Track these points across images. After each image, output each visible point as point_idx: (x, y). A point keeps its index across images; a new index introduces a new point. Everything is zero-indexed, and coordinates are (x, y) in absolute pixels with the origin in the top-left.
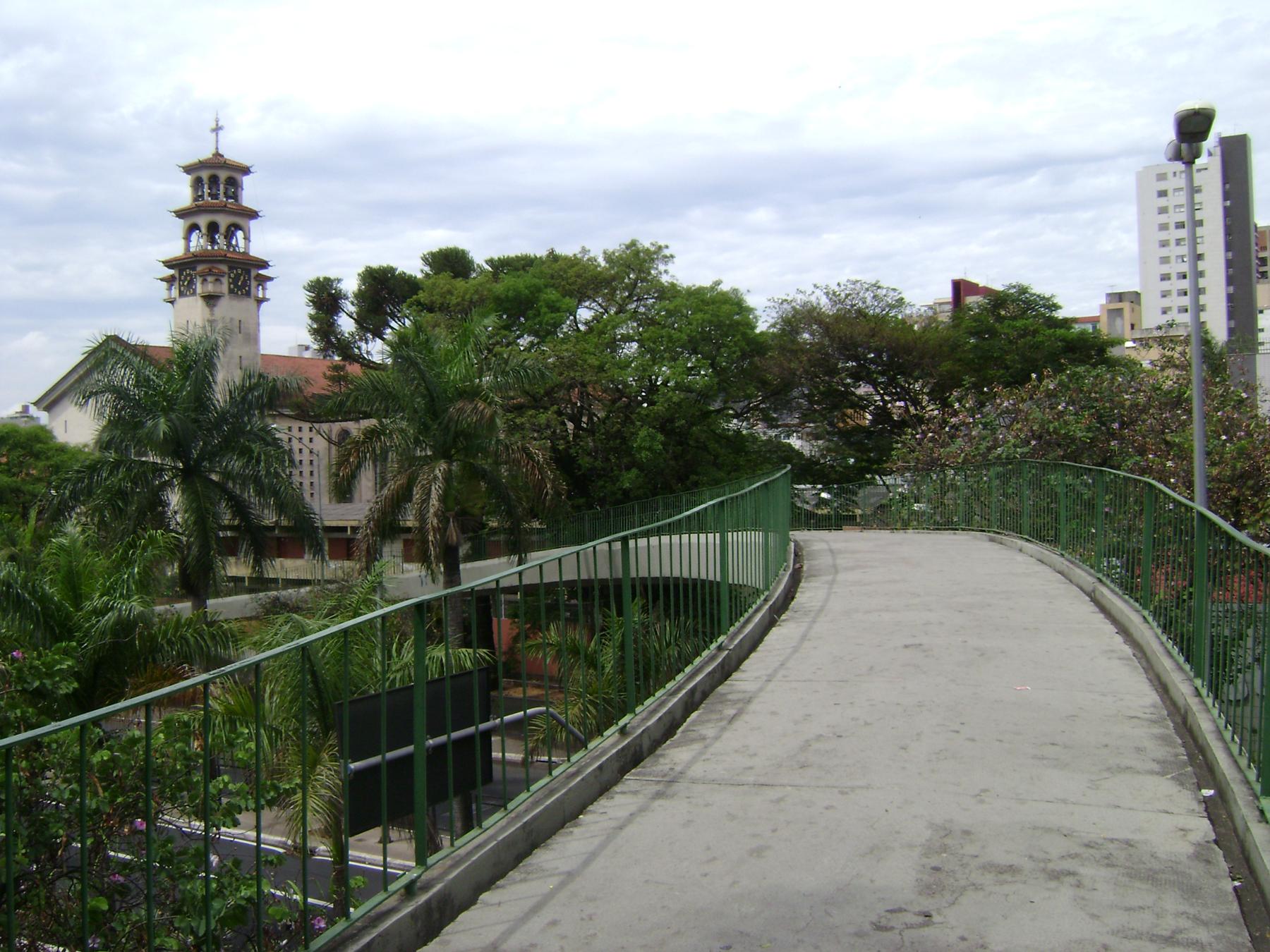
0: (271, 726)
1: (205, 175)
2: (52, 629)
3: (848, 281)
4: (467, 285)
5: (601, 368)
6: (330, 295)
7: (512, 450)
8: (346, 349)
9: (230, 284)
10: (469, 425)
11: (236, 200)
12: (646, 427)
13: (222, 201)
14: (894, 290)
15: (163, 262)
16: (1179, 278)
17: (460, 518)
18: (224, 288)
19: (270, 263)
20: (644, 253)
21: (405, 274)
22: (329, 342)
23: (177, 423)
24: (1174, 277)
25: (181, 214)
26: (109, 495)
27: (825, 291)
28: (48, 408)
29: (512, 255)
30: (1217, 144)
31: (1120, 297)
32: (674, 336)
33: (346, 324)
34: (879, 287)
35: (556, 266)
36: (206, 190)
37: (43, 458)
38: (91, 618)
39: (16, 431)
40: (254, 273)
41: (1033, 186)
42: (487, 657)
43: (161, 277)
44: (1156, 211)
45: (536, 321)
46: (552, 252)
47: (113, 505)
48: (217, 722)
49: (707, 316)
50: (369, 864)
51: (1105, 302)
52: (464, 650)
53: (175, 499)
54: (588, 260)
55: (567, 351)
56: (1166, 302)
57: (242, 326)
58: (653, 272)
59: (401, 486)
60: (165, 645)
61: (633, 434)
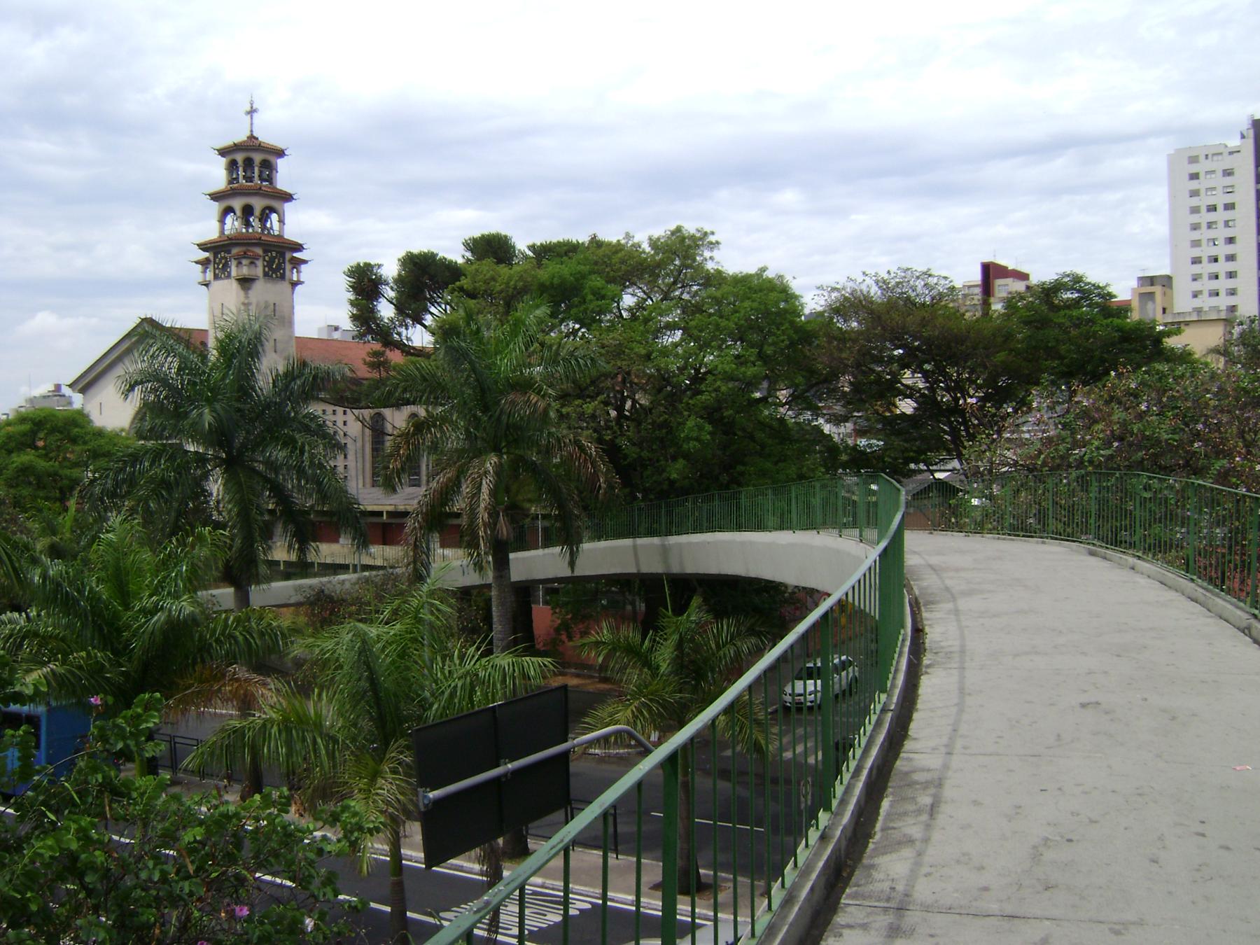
0: (328, 735)
1: (240, 157)
2: (101, 629)
3: (899, 269)
4: (512, 272)
5: (648, 357)
6: (371, 280)
7: (564, 443)
8: (384, 335)
9: (264, 266)
10: (522, 418)
11: (271, 183)
12: (693, 417)
13: (257, 184)
14: (945, 278)
15: (198, 245)
16: (1210, 261)
17: (510, 512)
18: (259, 271)
19: (304, 246)
20: (689, 239)
21: (446, 259)
22: (369, 327)
23: (222, 413)
24: (1205, 260)
25: (216, 197)
26: (153, 486)
27: (874, 278)
28: (83, 391)
29: (555, 240)
30: (1250, 126)
31: (1152, 280)
32: (722, 324)
33: (386, 310)
34: (930, 275)
35: (601, 252)
36: (241, 173)
37: (80, 442)
38: (138, 617)
39: (54, 416)
40: (288, 256)
41: (1060, 167)
42: (551, 666)
43: (196, 260)
44: (1187, 195)
45: (582, 309)
46: (594, 238)
47: (157, 495)
48: (273, 731)
49: (755, 305)
50: (415, 862)
51: (1136, 286)
52: (528, 658)
53: (216, 486)
54: (633, 245)
55: (611, 339)
56: (1197, 286)
57: (277, 308)
58: (698, 258)
59: (450, 480)
60: (214, 644)
61: (679, 424)
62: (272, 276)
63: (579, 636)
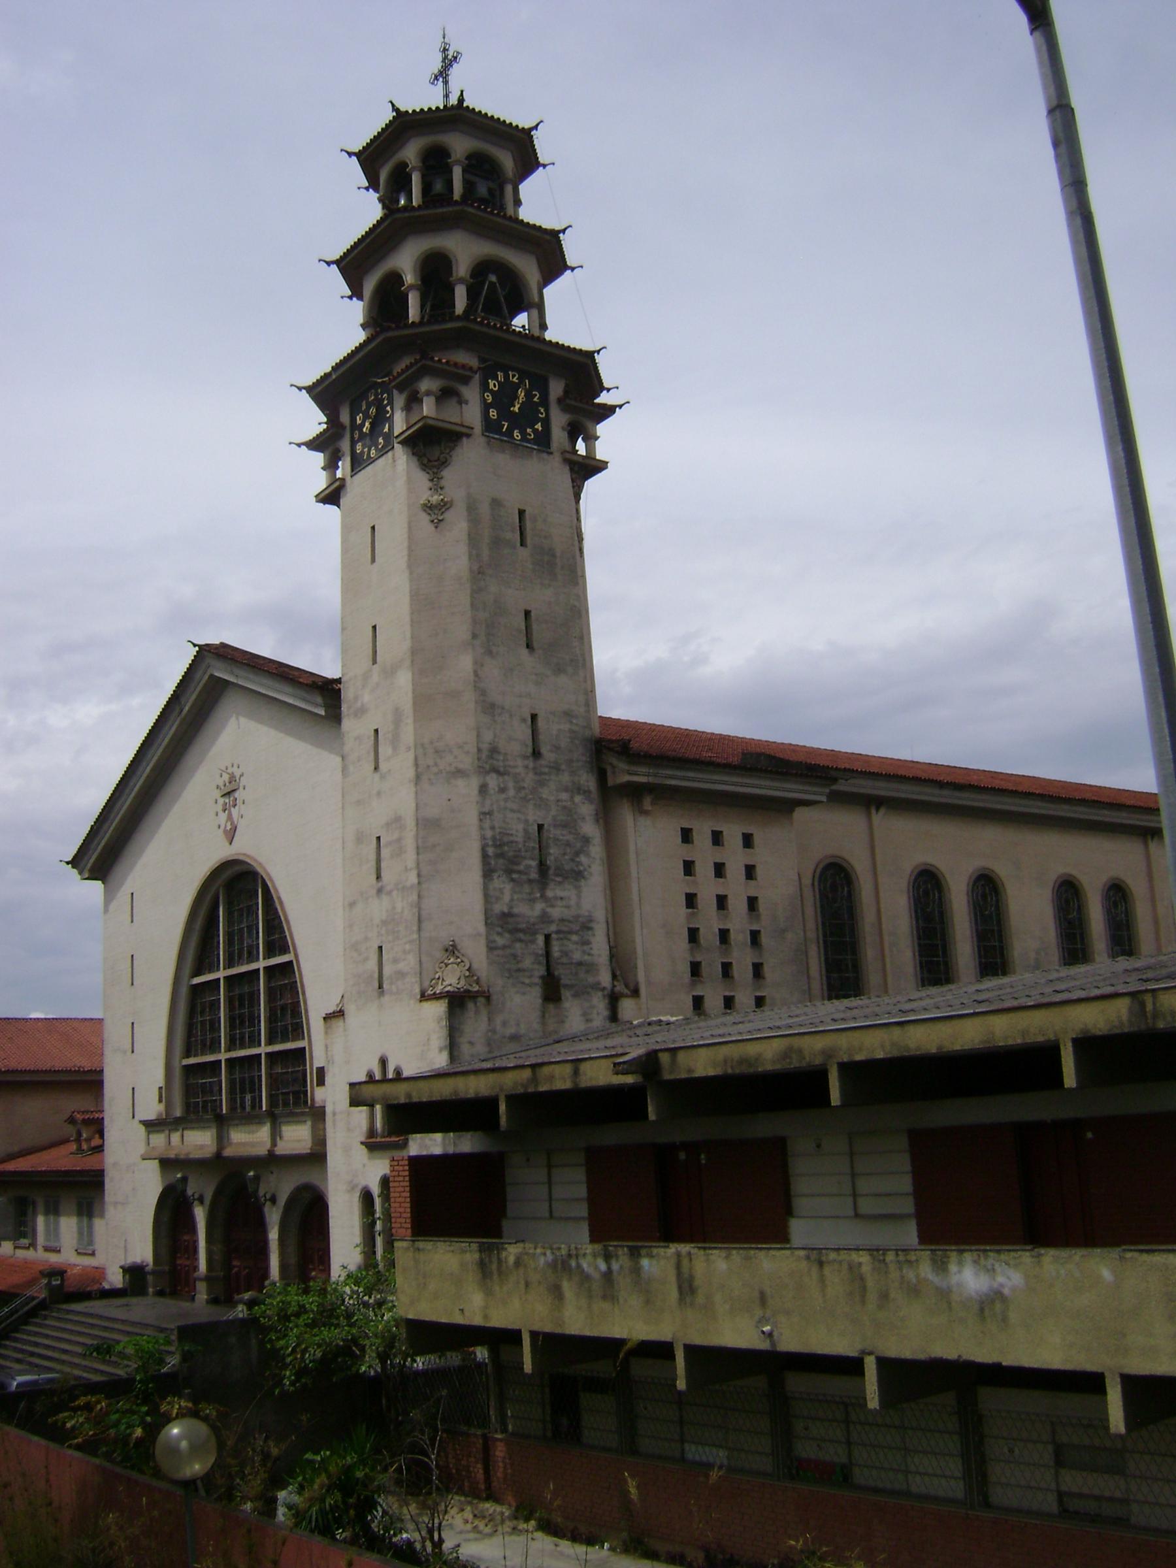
9: (486, 407)
57: (528, 525)
62: (509, 434)
63: (580, 919)
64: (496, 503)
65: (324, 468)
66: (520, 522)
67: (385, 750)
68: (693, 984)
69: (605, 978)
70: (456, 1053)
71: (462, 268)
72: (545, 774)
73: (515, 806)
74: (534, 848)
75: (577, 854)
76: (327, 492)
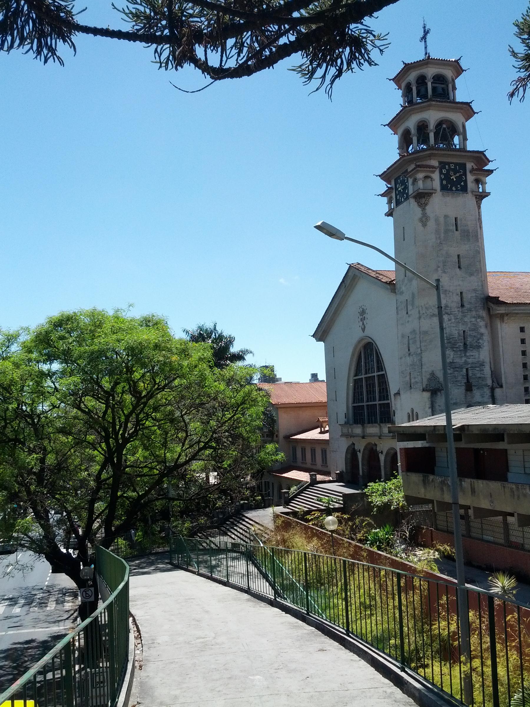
9: (441, 180)
57: (459, 222)
64: (446, 217)
65: (387, 204)
66: (456, 221)
67: (410, 307)
68: (525, 383)
69: (489, 382)
70: (434, 409)
71: (432, 126)
72: (466, 312)
73: (454, 325)
74: (462, 339)
75: (478, 340)
76: (388, 213)
